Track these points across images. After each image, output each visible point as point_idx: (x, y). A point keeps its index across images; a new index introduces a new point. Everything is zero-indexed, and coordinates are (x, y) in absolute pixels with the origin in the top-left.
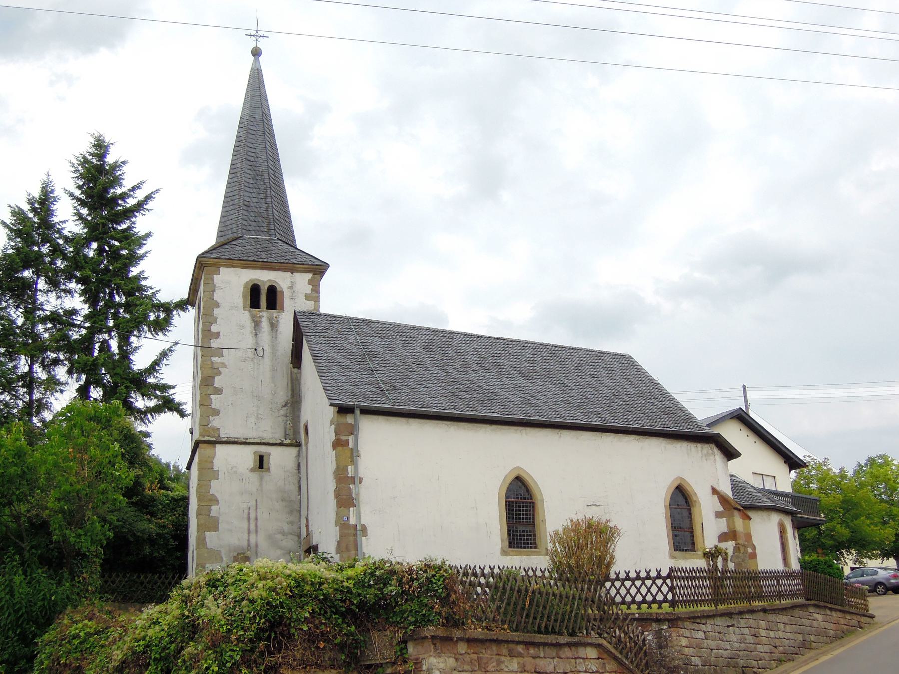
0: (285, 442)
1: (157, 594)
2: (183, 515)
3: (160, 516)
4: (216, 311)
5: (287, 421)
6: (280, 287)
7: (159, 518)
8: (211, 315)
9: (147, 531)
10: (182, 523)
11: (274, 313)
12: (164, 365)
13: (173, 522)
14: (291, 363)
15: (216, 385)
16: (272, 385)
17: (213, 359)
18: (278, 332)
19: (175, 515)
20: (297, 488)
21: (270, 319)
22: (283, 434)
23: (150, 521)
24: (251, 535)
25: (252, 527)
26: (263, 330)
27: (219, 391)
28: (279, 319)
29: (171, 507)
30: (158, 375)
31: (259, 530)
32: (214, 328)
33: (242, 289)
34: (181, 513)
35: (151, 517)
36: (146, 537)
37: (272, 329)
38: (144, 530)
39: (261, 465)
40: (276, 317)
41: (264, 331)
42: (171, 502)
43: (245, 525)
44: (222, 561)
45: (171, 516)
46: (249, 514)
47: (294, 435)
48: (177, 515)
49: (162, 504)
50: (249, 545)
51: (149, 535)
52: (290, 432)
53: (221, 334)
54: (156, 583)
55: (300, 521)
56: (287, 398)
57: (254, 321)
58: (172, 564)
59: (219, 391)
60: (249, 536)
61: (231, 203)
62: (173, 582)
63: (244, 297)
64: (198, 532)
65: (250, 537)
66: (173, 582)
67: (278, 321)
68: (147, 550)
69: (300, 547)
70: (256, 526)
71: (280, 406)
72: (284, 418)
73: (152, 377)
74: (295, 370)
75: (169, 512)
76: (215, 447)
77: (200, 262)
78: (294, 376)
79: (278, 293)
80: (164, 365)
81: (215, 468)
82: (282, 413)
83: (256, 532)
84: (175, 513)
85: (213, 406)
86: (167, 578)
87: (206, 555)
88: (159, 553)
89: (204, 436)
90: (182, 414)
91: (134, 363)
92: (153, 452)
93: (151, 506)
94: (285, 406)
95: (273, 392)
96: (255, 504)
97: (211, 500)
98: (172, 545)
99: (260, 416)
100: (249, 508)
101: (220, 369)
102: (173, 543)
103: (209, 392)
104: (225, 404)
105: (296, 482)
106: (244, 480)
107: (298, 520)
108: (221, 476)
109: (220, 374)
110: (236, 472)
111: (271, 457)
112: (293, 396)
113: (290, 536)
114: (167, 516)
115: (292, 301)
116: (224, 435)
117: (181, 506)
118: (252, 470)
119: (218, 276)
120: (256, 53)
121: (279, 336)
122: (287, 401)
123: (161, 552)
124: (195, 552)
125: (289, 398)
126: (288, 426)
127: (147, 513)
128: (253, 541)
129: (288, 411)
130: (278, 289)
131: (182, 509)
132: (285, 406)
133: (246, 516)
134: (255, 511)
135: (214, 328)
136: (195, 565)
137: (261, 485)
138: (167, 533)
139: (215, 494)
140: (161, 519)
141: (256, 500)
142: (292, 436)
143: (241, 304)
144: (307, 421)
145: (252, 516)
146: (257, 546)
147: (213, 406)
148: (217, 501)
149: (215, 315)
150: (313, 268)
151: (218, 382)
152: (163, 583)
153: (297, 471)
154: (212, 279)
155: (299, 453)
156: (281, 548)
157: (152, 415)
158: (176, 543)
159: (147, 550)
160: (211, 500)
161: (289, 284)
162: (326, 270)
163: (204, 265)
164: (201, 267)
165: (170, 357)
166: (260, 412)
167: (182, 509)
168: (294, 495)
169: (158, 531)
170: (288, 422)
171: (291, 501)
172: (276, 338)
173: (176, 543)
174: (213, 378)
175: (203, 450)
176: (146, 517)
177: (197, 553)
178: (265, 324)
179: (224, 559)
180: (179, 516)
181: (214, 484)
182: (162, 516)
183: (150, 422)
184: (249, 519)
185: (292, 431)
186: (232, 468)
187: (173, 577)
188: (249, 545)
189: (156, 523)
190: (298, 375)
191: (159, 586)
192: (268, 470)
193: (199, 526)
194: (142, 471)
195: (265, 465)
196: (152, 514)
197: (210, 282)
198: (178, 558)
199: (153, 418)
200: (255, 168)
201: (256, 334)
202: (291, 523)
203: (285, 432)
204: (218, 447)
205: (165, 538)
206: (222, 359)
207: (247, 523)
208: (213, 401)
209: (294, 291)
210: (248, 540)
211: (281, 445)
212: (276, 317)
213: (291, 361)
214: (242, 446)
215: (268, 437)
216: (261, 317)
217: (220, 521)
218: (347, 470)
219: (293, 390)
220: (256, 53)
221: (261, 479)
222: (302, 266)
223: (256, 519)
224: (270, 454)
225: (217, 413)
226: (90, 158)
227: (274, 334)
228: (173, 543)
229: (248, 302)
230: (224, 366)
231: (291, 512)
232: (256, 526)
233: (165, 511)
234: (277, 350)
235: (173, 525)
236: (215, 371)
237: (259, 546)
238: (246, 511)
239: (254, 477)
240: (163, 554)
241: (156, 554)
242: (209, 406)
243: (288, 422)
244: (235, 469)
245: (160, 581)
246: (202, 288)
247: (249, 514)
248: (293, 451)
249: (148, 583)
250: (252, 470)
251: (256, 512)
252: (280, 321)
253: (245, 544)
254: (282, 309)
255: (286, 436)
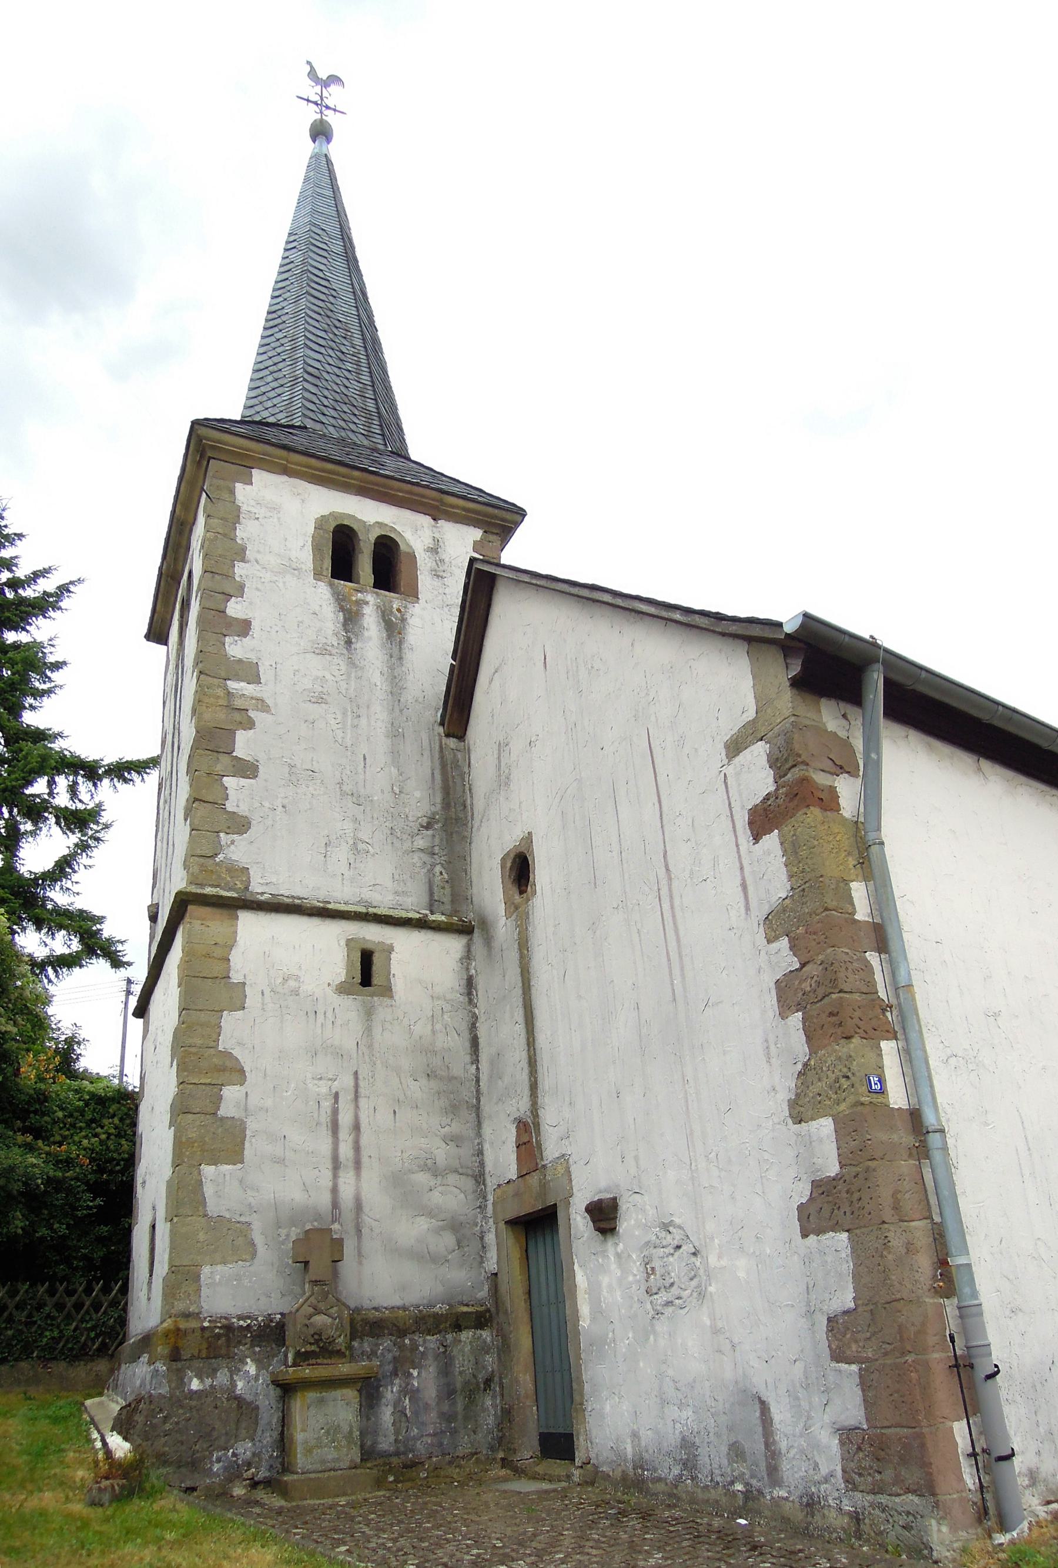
0: (432, 918)
1: (41, 1335)
2: (119, 1136)
3: (58, 1138)
4: (240, 570)
5: (433, 865)
6: (408, 545)
7: (54, 1143)
8: (229, 576)
9: (19, 1171)
10: (115, 1155)
11: (395, 601)
12: (82, 867)
13: (93, 1150)
14: (442, 724)
15: (239, 752)
16: (394, 771)
17: (232, 685)
18: (405, 646)
19: (96, 1135)
20: (468, 1044)
21: (383, 612)
22: (425, 899)
23: (30, 1148)
24: (341, 1173)
25: (346, 1150)
26: (366, 634)
27: (247, 770)
28: (408, 616)
29: (89, 1116)
30: (69, 884)
31: (365, 1160)
32: (235, 609)
33: (311, 529)
34: (112, 1131)
35: (36, 1138)
36: (16, 1187)
37: (390, 637)
38: (12, 1169)
39: (366, 980)
40: (399, 610)
41: (370, 638)
42: (87, 1105)
43: (324, 1146)
44: (254, 1255)
45: (86, 1137)
46: (335, 1112)
47: (452, 902)
48: (103, 1137)
49: (62, 1109)
50: (335, 1204)
51: (25, 1184)
52: (444, 895)
53: (255, 625)
54: (40, 1307)
55: (479, 1134)
56: (433, 809)
57: (342, 609)
58: (85, 1257)
59: (247, 770)
60: (335, 1176)
61: (270, 378)
62: (88, 1303)
63: (317, 548)
64: (176, 1165)
65: (341, 1181)
66: (88, 1303)
67: (403, 620)
68: (18, 1222)
69: (482, 1208)
70: (357, 1148)
71: (415, 826)
72: (426, 858)
73: (57, 888)
74: (452, 742)
75: (81, 1129)
76: (237, 918)
77: (200, 439)
78: (449, 756)
79: (403, 558)
80: (82, 867)
81: (236, 977)
82: (420, 843)
83: (358, 1165)
84: (99, 1130)
85: (230, 806)
86: (70, 1293)
87: (202, 1236)
88: (51, 1228)
89: (202, 885)
90: (117, 963)
91: (22, 862)
92: (50, 1011)
93: (36, 1112)
94: (428, 827)
95: (397, 790)
96: (352, 1083)
97: (222, 1069)
98: (89, 1208)
99: (361, 846)
100: (336, 1096)
101: (252, 714)
102: (90, 1202)
103: (219, 768)
104: (267, 804)
105: (464, 1027)
106: (320, 1016)
107: (471, 1133)
108: (252, 999)
109: (250, 725)
110: (296, 993)
111: (393, 956)
112: (446, 805)
113: (452, 1178)
114: (76, 1138)
115: (437, 583)
116: (260, 887)
117: (113, 1116)
118: (343, 989)
119: (248, 487)
120: (321, 132)
121: (408, 656)
122: (434, 814)
123: (56, 1226)
124: (163, 1230)
125: (439, 807)
126: (438, 879)
127: (24, 1131)
128: (347, 1192)
129: (437, 841)
130: (403, 547)
131: (116, 1121)
132: (428, 827)
133: (325, 1118)
134: (352, 1107)
135: (235, 609)
136: (162, 1268)
137: (368, 1030)
138: (77, 1179)
139: (235, 1053)
140: (60, 1144)
141: (356, 1073)
142: (448, 907)
143: (309, 565)
144: (528, 839)
145: (345, 1119)
146: (359, 1206)
147: (230, 806)
148: (242, 1071)
149: (238, 579)
150: (486, 515)
151: (244, 745)
152: (60, 1307)
153: (464, 999)
154: (232, 492)
155: (469, 951)
156: (430, 1214)
157: (56, 971)
158: (99, 1201)
159: (18, 1222)
160: (222, 1069)
161: (429, 542)
162: (517, 524)
163: (209, 454)
164: (199, 463)
165: (95, 850)
166: (363, 835)
167: (116, 1121)
168: (460, 1064)
169: (51, 1173)
170: (438, 869)
171: (452, 1079)
172: (401, 658)
173: (99, 1201)
174: (232, 733)
175: (196, 919)
176: (20, 1138)
177: (173, 1233)
178: (370, 618)
179: (261, 1249)
180: (108, 1138)
181: (229, 1021)
182: (65, 1138)
183: (50, 981)
184: (335, 1127)
185: (448, 891)
186: (285, 980)
187: (88, 1291)
188: (335, 1204)
189: (48, 1154)
190: (459, 755)
191: (48, 1316)
192: (387, 991)
193: (180, 1146)
194: (15, 1024)
195: (375, 980)
196: (38, 1133)
197: (226, 496)
198: (101, 1240)
199: (57, 976)
200: (329, 313)
201: (349, 642)
202: (454, 1139)
203: (431, 894)
204: (246, 918)
205: (69, 1191)
206: (258, 688)
207: (329, 1140)
208: (230, 792)
209: (442, 561)
210: (335, 1190)
211: (421, 924)
212: (399, 610)
213: (443, 716)
214: (315, 921)
215: (384, 902)
216: (360, 603)
217: (248, 1132)
218: (851, 898)
219: (447, 790)
220: (321, 132)
221: (369, 1013)
222: (461, 502)
223: (357, 1127)
224: (390, 949)
225: (240, 825)
226: (19, 931)
227: (396, 650)
228: (90, 1202)
229: (328, 564)
230: (263, 705)
231: (453, 1109)
232: (357, 1148)
233: (73, 1126)
234: (402, 688)
235: (92, 1160)
236: (237, 716)
237: (366, 1209)
238: (327, 1105)
239: (349, 1008)
240: (63, 1230)
241: (43, 1232)
242: (219, 805)
243: (438, 869)
244: (292, 983)
245: (50, 1302)
246: (201, 520)
247: (335, 1112)
248: (453, 946)
249: (17, 1307)
250: (343, 989)
251: (357, 1107)
252: (411, 621)
253: (324, 1200)
254: (413, 594)
255: (432, 904)
